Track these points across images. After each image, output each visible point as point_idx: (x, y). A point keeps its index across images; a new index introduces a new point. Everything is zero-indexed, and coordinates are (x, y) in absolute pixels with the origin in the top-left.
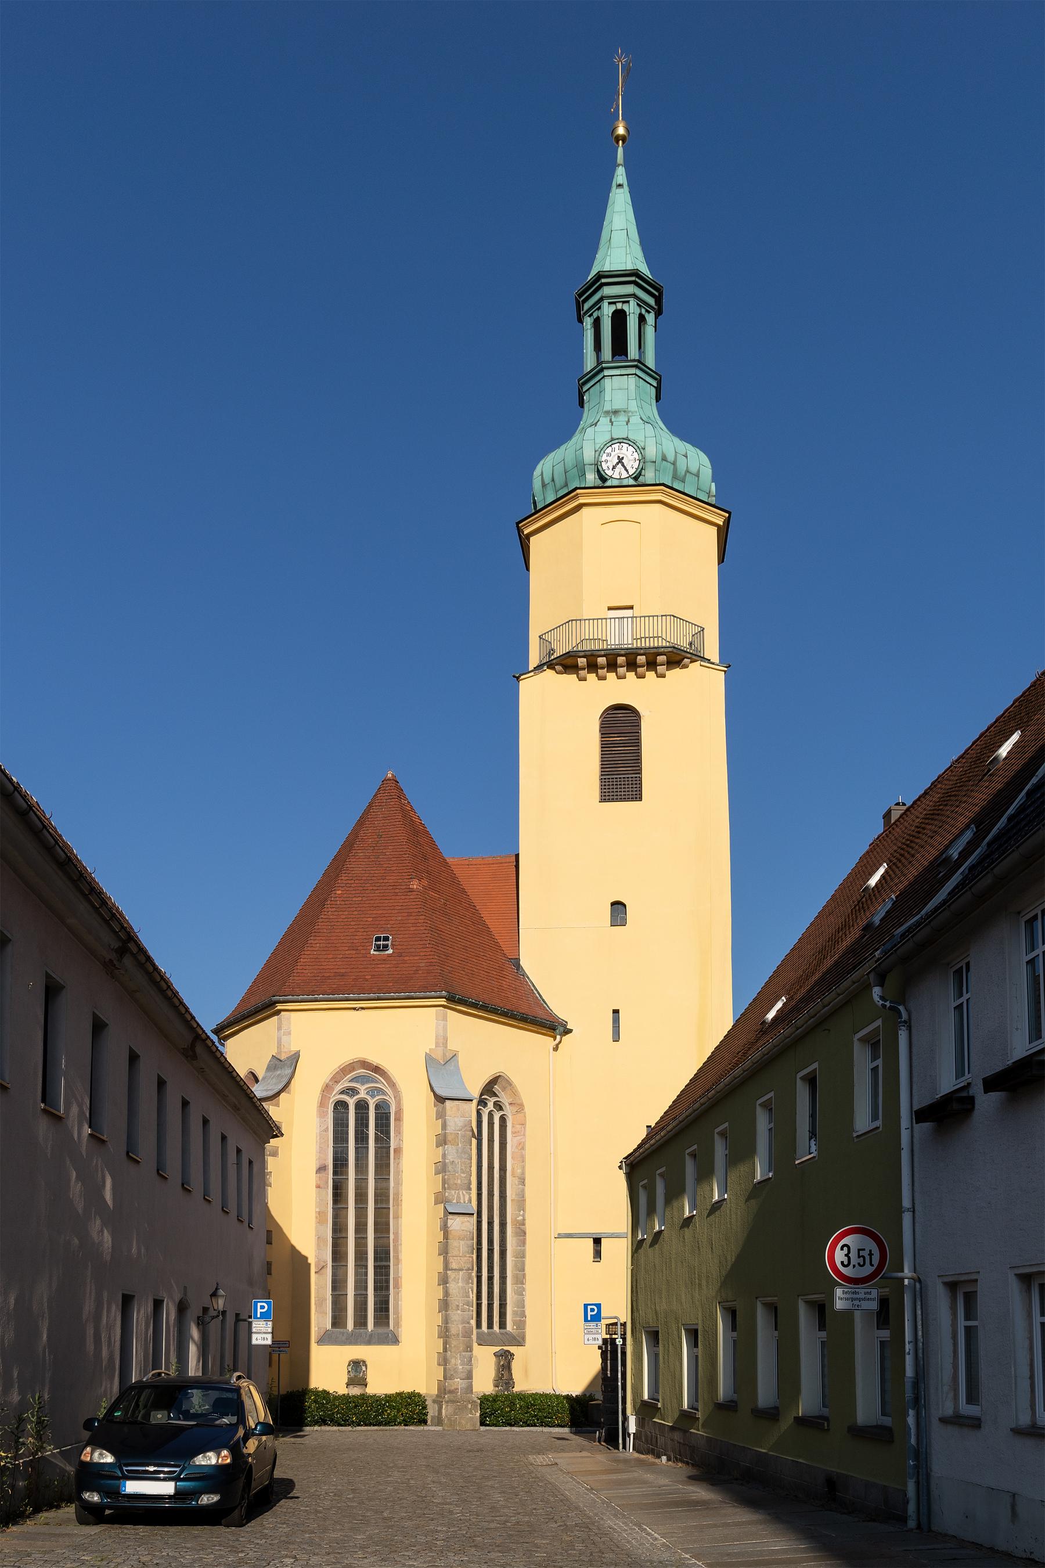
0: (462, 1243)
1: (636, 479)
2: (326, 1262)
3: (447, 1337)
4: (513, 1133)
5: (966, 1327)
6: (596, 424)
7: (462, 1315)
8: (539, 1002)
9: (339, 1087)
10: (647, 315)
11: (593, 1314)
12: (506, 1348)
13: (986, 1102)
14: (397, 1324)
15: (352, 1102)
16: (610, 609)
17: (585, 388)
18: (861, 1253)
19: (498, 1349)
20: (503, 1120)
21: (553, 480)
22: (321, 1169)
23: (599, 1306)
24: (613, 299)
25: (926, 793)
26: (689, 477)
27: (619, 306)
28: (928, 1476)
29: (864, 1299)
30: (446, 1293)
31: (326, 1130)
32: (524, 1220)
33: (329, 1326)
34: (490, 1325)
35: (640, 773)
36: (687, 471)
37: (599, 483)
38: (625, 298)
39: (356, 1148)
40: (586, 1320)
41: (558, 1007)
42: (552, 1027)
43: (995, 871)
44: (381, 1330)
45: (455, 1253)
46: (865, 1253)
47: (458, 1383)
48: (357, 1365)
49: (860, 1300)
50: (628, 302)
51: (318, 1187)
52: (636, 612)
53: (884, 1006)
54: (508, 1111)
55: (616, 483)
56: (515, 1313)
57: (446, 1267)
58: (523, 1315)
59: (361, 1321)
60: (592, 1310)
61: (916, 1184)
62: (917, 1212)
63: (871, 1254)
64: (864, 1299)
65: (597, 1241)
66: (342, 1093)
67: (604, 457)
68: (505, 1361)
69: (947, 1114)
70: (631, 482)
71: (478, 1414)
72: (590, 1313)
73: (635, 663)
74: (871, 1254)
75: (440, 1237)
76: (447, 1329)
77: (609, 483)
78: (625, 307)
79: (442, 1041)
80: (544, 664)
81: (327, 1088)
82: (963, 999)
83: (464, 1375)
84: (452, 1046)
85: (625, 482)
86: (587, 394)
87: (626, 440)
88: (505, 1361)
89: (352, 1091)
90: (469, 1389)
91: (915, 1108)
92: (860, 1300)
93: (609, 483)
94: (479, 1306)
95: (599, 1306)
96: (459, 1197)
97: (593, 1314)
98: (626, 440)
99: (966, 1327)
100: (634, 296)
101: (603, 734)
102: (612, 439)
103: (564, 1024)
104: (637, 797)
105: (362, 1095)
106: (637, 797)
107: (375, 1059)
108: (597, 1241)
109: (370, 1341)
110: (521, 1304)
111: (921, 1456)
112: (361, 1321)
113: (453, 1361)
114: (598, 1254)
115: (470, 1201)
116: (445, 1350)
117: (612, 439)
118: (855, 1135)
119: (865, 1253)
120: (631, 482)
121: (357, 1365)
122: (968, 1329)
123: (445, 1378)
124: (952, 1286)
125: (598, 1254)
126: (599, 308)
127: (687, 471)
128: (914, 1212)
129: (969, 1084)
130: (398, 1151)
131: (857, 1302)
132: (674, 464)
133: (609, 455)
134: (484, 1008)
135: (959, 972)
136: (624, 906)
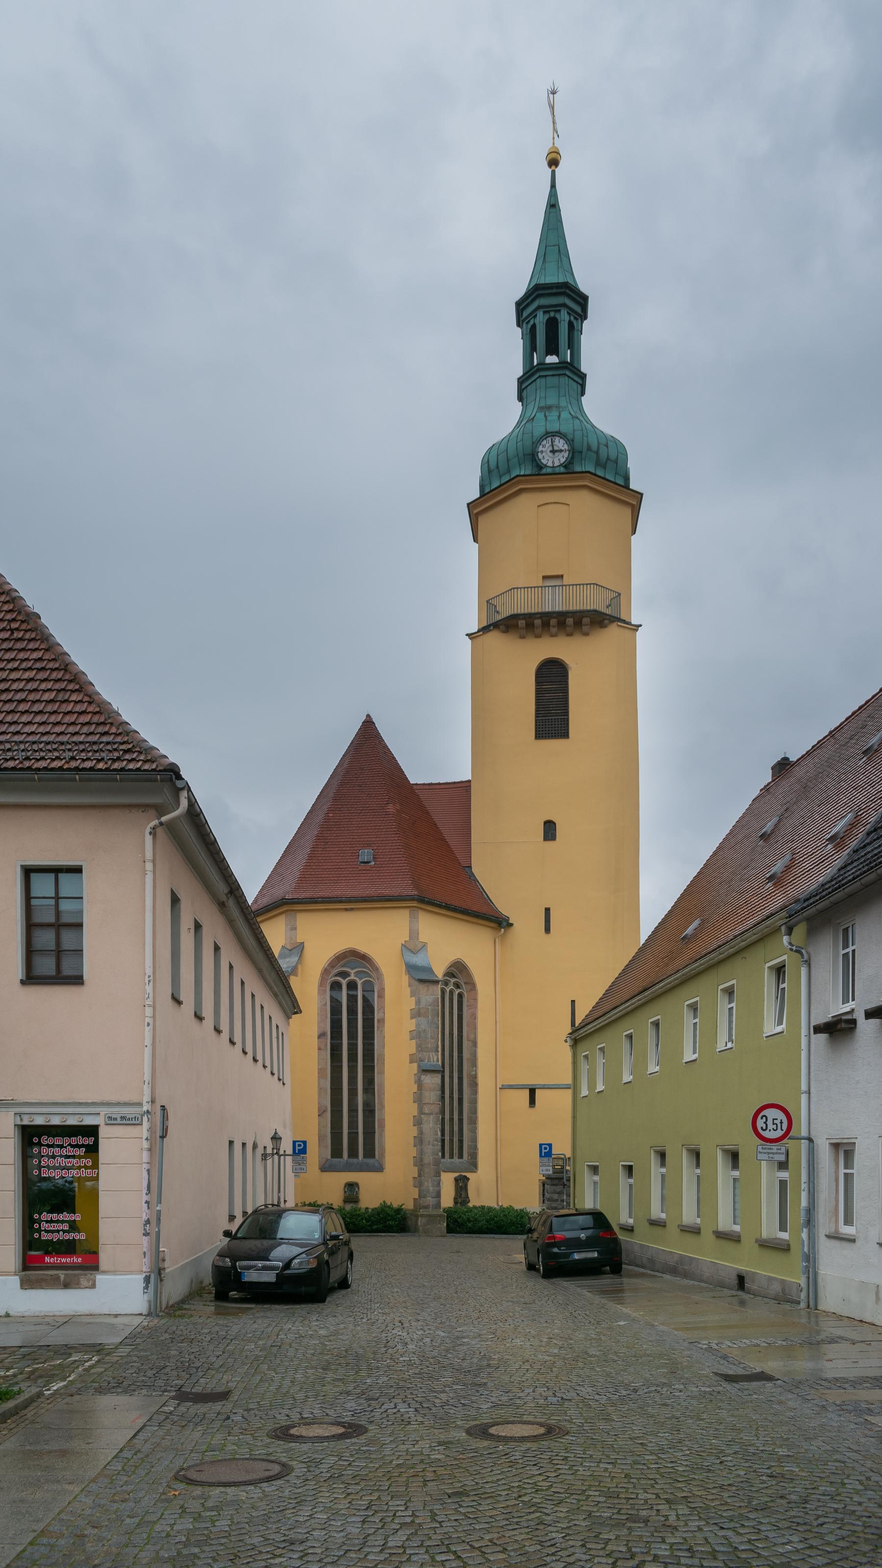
0: (432, 1093)
1: (565, 467)
2: (326, 1107)
3: (422, 1165)
4: (468, 1006)
5: (845, 1174)
6: (533, 419)
7: (431, 1150)
8: (488, 901)
9: (335, 971)
10: (575, 322)
11: (546, 1151)
12: (463, 1174)
13: (866, 1027)
14: (382, 1155)
15: (344, 982)
16: (544, 578)
17: (523, 386)
18: (775, 1121)
19: (457, 1174)
20: (460, 996)
21: (497, 467)
22: (321, 1035)
23: (550, 1145)
24: (546, 309)
25: (808, 753)
26: (610, 465)
27: (552, 314)
28: (816, 1274)
29: (776, 1153)
30: (421, 1132)
31: (325, 1005)
32: (476, 1074)
33: (329, 1157)
34: (452, 1157)
35: (568, 715)
36: (608, 459)
37: (535, 471)
38: (557, 308)
39: (348, 1019)
40: (541, 1156)
41: (503, 906)
42: (499, 922)
43: (878, 871)
44: (370, 1161)
45: (427, 1101)
46: (778, 1122)
47: (430, 1200)
48: (351, 1186)
49: (773, 1154)
50: (559, 311)
51: (319, 1049)
52: (566, 581)
53: (791, 950)
54: (464, 990)
55: (549, 470)
56: (469, 1147)
57: (421, 1111)
58: (476, 1148)
59: (353, 1153)
60: (545, 1148)
61: (812, 1075)
62: (812, 1095)
63: (781, 1123)
64: (776, 1153)
65: (532, 1092)
66: (336, 975)
67: (541, 448)
68: (461, 1184)
69: (838, 1029)
70: (562, 470)
71: (445, 1224)
72: (543, 1151)
73: (565, 623)
74: (781, 1123)
75: (415, 1088)
76: (422, 1160)
77: (544, 471)
78: (557, 316)
79: (414, 934)
80: (490, 625)
81: (326, 972)
82: (850, 949)
83: (434, 1194)
84: (423, 938)
85: (557, 470)
86: (525, 392)
87: (559, 434)
88: (461, 1184)
89: (344, 975)
90: (438, 1205)
91: (813, 1024)
92: (773, 1154)
93: (544, 471)
94: (443, 1141)
95: (550, 1145)
96: (429, 1057)
97: (546, 1151)
98: (559, 434)
99: (845, 1174)
100: (564, 305)
101: (538, 683)
102: (547, 433)
103: (507, 919)
104: (565, 735)
105: (352, 977)
106: (565, 735)
107: (363, 949)
108: (532, 1092)
109: (361, 1168)
110: (474, 1140)
111: (810, 1260)
112: (353, 1153)
113: (426, 1184)
114: (532, 1102)
115: (438, 1061)
116: (420, 1175)
117: (547, 433)
118: (765, 1035)
119: (778, 1122)
120: (562, 470)
121: (351, 1186)
122: (846, 1175)
123: (420, 1196)
124: (836, 1146)
125: (532, 1102)
126: (536, 316)
127: (608, 459)
128: (809, 1093)
129: (853, 1010)
130: (382, 1021)
131: (771, 1155)
132: (597, 453)
133: (543, 446)
134: (448, 907)
135: (846, 931)
136: (555, 824)
